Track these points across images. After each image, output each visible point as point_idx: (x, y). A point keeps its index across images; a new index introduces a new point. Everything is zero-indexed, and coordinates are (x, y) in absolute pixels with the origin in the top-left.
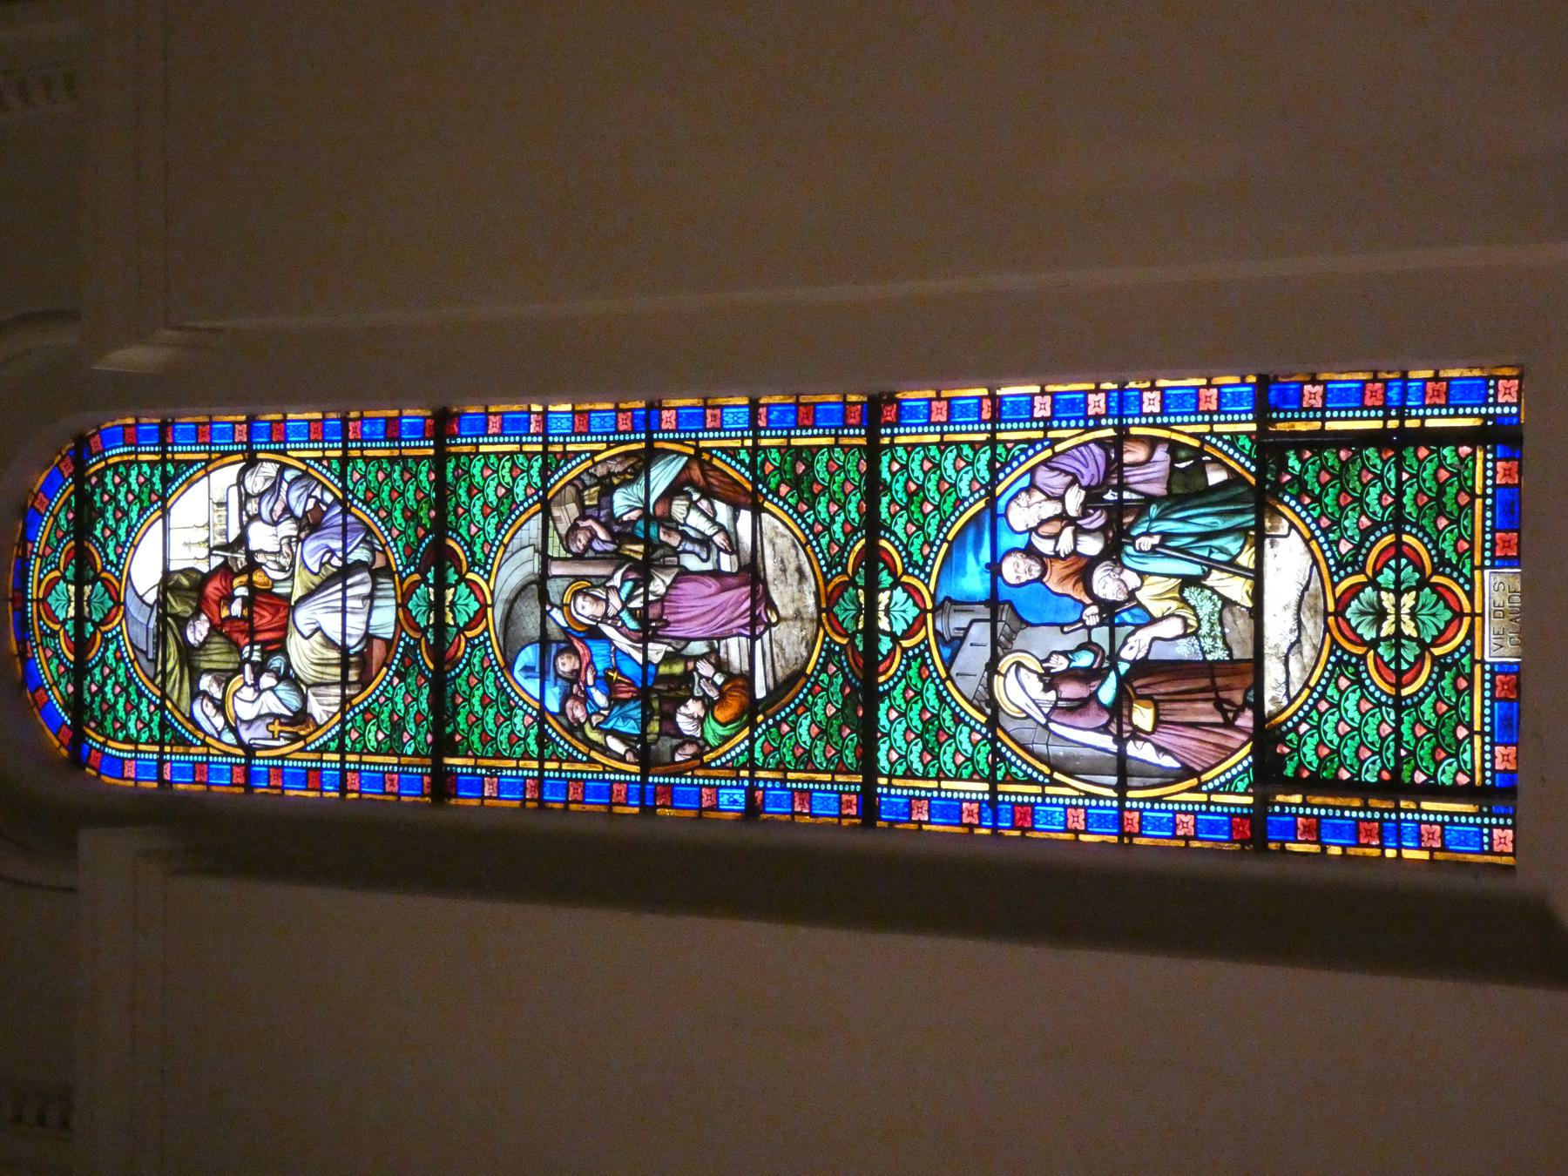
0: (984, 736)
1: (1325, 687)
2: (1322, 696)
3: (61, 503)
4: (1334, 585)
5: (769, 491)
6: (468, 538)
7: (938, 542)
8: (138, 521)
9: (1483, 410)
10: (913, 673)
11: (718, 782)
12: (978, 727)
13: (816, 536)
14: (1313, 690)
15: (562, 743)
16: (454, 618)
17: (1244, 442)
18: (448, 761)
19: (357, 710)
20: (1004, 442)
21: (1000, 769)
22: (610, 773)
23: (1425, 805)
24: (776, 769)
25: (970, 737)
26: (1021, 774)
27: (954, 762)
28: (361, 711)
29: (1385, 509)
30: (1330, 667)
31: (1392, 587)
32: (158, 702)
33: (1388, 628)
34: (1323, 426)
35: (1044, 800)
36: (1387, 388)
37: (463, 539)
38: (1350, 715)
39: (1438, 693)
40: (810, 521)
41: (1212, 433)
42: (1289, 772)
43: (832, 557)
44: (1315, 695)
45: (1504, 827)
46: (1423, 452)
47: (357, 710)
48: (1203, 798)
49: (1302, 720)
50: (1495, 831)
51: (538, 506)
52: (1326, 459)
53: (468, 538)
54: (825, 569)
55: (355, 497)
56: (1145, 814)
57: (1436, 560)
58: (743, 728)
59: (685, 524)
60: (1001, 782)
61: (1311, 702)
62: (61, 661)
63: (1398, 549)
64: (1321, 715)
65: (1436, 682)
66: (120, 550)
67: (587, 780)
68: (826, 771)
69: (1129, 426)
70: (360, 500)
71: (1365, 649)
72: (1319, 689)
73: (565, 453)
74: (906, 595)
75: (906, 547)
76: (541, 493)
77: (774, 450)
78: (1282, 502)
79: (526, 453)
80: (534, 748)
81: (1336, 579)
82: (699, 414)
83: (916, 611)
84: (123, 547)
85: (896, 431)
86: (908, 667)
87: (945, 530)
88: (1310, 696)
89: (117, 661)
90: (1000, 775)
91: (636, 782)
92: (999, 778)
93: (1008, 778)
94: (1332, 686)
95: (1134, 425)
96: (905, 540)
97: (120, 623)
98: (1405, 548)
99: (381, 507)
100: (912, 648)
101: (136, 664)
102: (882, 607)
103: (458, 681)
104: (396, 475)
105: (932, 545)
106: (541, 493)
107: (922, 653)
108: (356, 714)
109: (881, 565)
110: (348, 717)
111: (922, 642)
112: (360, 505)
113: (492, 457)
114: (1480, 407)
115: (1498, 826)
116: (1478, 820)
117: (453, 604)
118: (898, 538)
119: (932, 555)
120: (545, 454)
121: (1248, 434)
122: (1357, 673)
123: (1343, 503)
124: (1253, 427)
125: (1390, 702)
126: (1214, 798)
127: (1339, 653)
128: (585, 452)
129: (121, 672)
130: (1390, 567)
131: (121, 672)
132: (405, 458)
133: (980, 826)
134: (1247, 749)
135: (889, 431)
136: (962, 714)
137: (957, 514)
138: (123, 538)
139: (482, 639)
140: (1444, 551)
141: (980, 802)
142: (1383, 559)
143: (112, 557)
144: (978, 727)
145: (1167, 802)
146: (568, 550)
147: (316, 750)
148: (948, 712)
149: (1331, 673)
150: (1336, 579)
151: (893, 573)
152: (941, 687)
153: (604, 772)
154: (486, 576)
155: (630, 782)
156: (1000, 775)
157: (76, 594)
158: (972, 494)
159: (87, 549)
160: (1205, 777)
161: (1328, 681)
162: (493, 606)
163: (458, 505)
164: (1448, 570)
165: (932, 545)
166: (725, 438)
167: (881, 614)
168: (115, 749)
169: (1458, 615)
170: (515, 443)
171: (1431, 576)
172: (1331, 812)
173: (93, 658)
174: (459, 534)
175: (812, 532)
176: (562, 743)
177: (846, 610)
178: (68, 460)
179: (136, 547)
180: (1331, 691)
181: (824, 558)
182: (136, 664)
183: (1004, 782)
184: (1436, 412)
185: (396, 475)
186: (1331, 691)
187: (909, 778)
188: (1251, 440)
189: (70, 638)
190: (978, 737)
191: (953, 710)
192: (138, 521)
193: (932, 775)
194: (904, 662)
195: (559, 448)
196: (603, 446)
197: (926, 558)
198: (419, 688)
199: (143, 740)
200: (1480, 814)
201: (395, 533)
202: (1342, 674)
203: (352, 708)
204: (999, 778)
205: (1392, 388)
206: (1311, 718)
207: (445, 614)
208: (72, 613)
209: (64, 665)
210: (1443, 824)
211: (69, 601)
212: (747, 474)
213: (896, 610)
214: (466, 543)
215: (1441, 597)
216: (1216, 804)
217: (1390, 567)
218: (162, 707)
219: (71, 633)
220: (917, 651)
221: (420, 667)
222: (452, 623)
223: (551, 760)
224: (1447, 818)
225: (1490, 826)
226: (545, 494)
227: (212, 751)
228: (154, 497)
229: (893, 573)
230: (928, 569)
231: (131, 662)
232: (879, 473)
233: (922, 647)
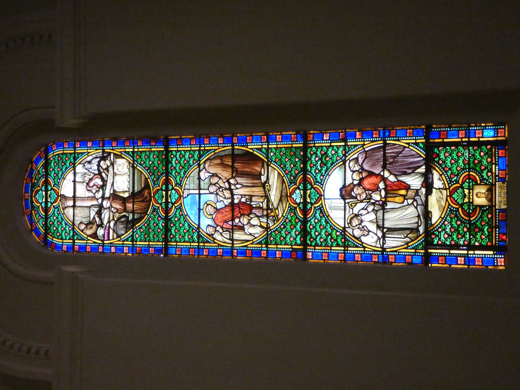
0: (341, 233)
1: (151, 215)
2: (150, 217)
3: (41, 164)
4: (289, 189)
5: (138, 163)
6: (175, 176)
7: (326, 175)
8: (65, 171)
9: (371, 139)
10: (317, 215)
11: (94, 244)
12: (71, 226)
13: (446, 172)
14: (284, 217)
15: (350, 240)
16: (171, 200)
17: (421, 145)
18: (430, 251)
19: (137, 228)
20: (77, 153)
21: (200, 239)
22: (220, 246)
23: (476, 252)
24: (274, 245)
25: (68, 229)
26: (352, 244)
27: (290, 240)
28: (139, 228)
29: (43, 172)
30: (288, 211)
31: (467, 188)
32: (72, 227)
33: (466, 200)
34: (443, 140)
35: (331, 251)
36: (379, 132)
37: (173, 176)
38: (323, 223)
39: (482, 219)
40: (285, 170)
41: (125, 152)
42: (435, 243)
43: (291, 180)
44: (285, 218)
45: (501, 258)
46: (476, 148)
47: (137, 228)
48: (122, 243)
49: (439, 228)
50: (498, 259)
51: (72, 168)
52: (447, 149)
53: (175, 176)
54: (289, 184)
55: (272, 161)
56: (283, 252)
57: (481, 178)
58: (265, 232)
59: (115, 174)
60: (200, 243)
61: (284, 220)
62: (159, 215)
63: (469, 177)
64: (445, 226)
65: (315, 214)
66: (59, 180)
67: (209, 248)
68: (188, 242)
69: (105, 149)
70: (274, 162)
71: (297, 205)
72: (286, 217)
73: (205, 150)
74: (175, 192)
75: (315, 177)
76: (198, 162)
77: (420, 144)
78: (434, 164)
79: (193, 150)
80: (196, 239)
81: (450, 185)
82: (216, 139)
83: (178, 196)
84: (60, 180)
85: (417, 138)
86: (176, 212)
87: (328, 171)
88: (284, 219)
89: (58, 215)
90: (200, 241)
91: (131, 247)
92: (200, 242)
93: (77, 239)
94: (289, 215)
95: (106, 149)
96: (53, 178)
97: (59, 203)
98: (471, 176)
99: (146, 166)
100: (177, 206)
101: (64, 215)
102: (308, 195)
103: (51, 218)
104: (151, 157)
105: (323, 176)
106: (198, 162)
107: (180, 207)
108: (137, 229)
109: (307, 182)
110: (134, 231)
111: (321, 205)
112: (274, 163)
113: (147, 152)
114: (370, 138)
115: (499, 258)
116: (493, 256)
117: (170, 195)
118: (52, 177)
119: (324, 179)
120: (199, 150)
121: (422, 143)
122: (295, 212)
123: (180, 169)
124: (424, 141)
125: (467, 222)
126: (124, 243)
127: (154, 206)
128: (212, 149)
129: (60, 217)
130: (467, 182)
131: (60, 217)
132: (180, 151)
133: (128, 253)
134: (424, 235)
135: (204, 146)
136: (67, 223)
137: (66, 171)
138: (183, 175)
139: (57, 206)
140: (317, 179)
141: (195, 248)
142: (465, 179)
143: (179, 182)
144: (71, 226)
145: (114, 244)
146: (450, 176)
147: (122, 241)
148: (64, 222)
149: (289, 212)
150: (290, 187)
151: (311, 184)
152: (185, 217)
153: (218, 246)
154: (321, 186)
155: (130, 247)
156: (200, 241)
157: (165, 194)
158: (194, 164)
159: (170, 179)
160: (122, 237)
161: (288, 214)
162: (447, 196)
163: (172, 166)
164: (318, 184)
165: (323, 176)
166: (186, 147)
167: (308, 197)
168: (57, 241)
169: (321, 195)
170: (260, 145)
171: (460, 184)
172: (226, 248)
173: (50, 215)
174: (172, 175)
175: (285, 173)
176: (350, 240)
177: (53, 196)
178: (43, 153)
179: (329, 176)
180: (152, 215)
181: (289, 180)
182: (64, 215)
183: (76, 240)
184: (140, 147)
185: (151, 157)
186: (152, 215)
187: (158, 242)
188: (423, 145)
189: (164, 209)
190: (71, 229)
191: (188, 223)
192: (65, 171)
193: (313, 245)
194: (175, 210)
195: (203, 148)
196: (217, 148)
197: (322, 180)
198: (297, 223)
199: (138, 241)
200: (494, 254)
201: (287, 172)
202: (291, 212)
203: (136, 228)
204: (200, 242)
205: (381, 132)
206: (442, 227)
207: (168, 199)
208: (44, 200)
209: (160, 217)
210: (482, 258)
211: (43, 197)
212: (132, 159)
213: (297, 196)
214: (53, 179)
215: (176, 192)
216: (125, 244)
217: (467, 182)
218: (73, 228)
219: (43, 207)
220: (179, 207)
221: (39, 214)
222: (170, 201)
223: (201, 243)
224: (483, 256)
225: (497, 258)
226: (200, 162)
227: (366, 249)
228: (195, 162)
229: (311, 184)
230: (59, 185)
231: (63, 214)
232: (307, 154)
233: (180, 205)
